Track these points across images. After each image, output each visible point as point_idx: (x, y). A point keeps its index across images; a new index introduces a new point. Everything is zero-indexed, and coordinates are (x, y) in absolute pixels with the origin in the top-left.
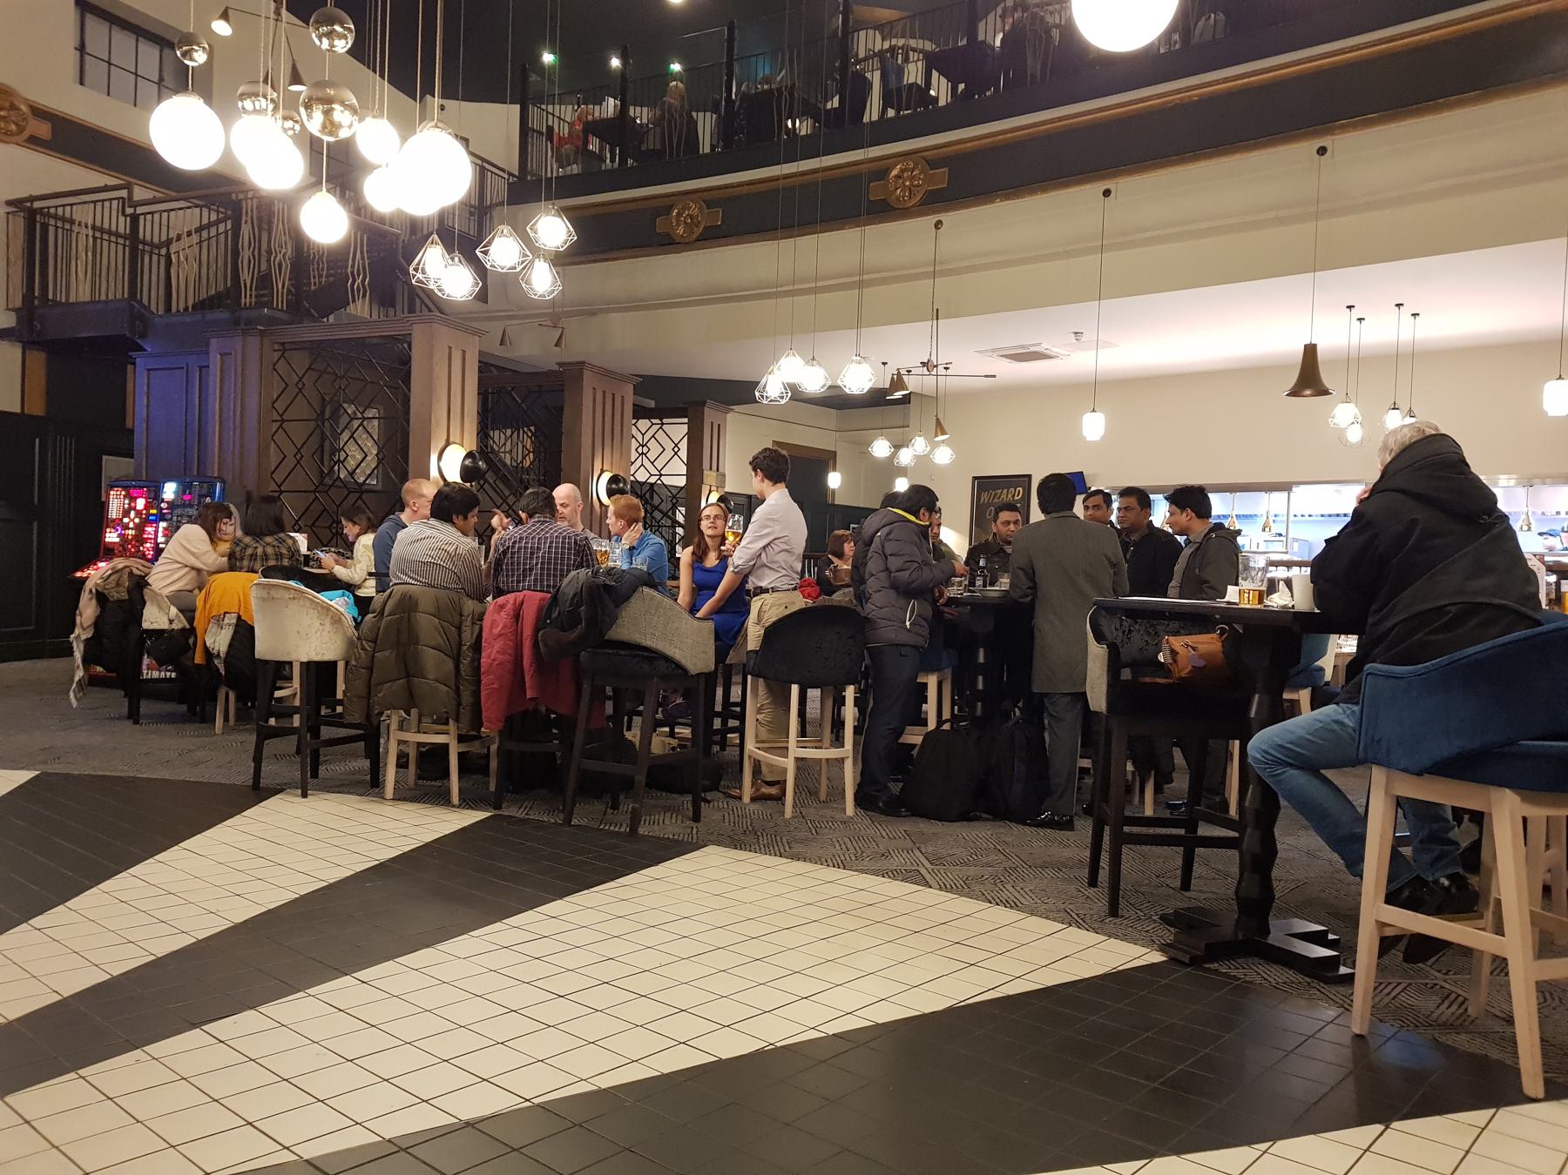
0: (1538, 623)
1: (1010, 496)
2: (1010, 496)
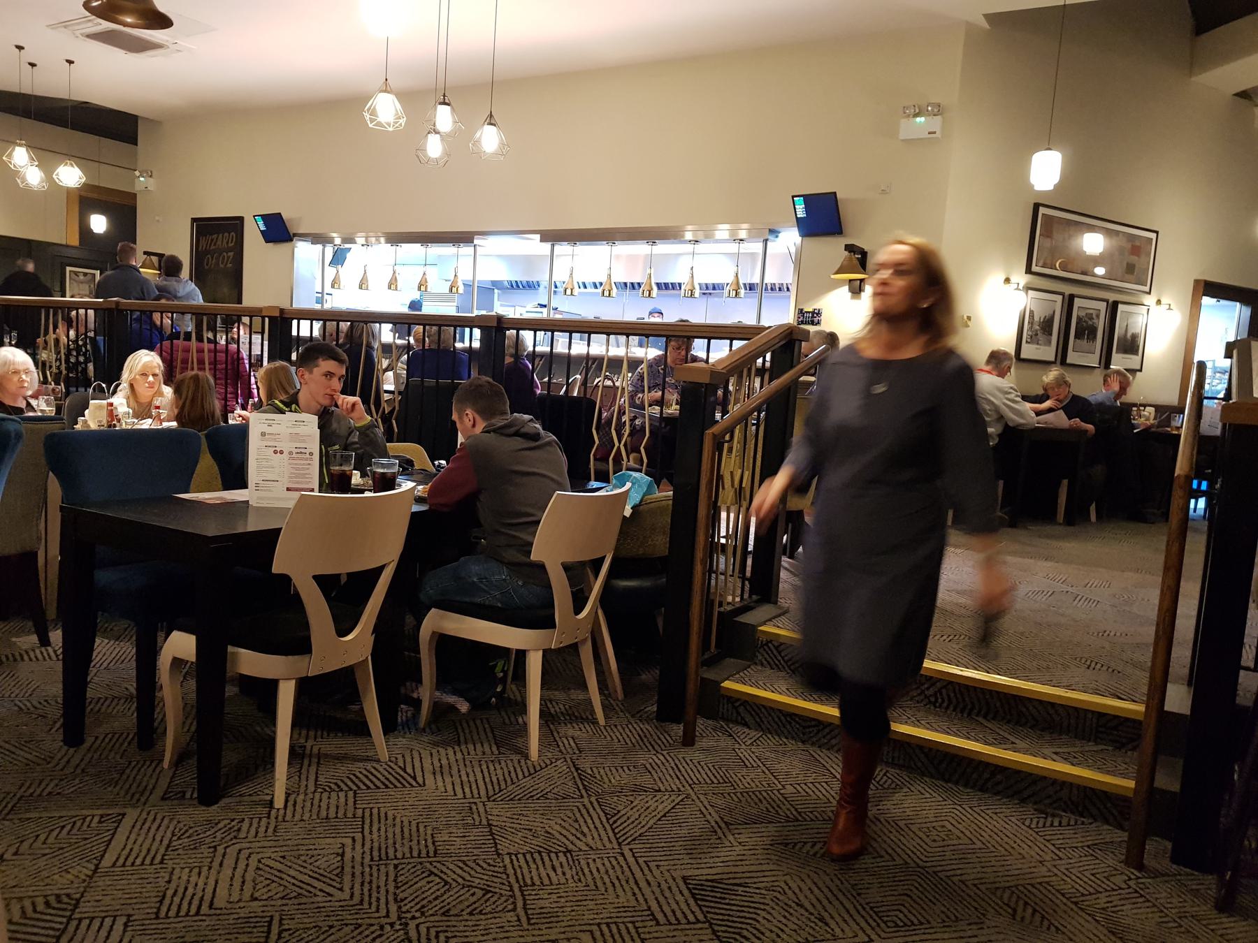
0: (176, 297)
1: (225, 241)
2: (225, 241)
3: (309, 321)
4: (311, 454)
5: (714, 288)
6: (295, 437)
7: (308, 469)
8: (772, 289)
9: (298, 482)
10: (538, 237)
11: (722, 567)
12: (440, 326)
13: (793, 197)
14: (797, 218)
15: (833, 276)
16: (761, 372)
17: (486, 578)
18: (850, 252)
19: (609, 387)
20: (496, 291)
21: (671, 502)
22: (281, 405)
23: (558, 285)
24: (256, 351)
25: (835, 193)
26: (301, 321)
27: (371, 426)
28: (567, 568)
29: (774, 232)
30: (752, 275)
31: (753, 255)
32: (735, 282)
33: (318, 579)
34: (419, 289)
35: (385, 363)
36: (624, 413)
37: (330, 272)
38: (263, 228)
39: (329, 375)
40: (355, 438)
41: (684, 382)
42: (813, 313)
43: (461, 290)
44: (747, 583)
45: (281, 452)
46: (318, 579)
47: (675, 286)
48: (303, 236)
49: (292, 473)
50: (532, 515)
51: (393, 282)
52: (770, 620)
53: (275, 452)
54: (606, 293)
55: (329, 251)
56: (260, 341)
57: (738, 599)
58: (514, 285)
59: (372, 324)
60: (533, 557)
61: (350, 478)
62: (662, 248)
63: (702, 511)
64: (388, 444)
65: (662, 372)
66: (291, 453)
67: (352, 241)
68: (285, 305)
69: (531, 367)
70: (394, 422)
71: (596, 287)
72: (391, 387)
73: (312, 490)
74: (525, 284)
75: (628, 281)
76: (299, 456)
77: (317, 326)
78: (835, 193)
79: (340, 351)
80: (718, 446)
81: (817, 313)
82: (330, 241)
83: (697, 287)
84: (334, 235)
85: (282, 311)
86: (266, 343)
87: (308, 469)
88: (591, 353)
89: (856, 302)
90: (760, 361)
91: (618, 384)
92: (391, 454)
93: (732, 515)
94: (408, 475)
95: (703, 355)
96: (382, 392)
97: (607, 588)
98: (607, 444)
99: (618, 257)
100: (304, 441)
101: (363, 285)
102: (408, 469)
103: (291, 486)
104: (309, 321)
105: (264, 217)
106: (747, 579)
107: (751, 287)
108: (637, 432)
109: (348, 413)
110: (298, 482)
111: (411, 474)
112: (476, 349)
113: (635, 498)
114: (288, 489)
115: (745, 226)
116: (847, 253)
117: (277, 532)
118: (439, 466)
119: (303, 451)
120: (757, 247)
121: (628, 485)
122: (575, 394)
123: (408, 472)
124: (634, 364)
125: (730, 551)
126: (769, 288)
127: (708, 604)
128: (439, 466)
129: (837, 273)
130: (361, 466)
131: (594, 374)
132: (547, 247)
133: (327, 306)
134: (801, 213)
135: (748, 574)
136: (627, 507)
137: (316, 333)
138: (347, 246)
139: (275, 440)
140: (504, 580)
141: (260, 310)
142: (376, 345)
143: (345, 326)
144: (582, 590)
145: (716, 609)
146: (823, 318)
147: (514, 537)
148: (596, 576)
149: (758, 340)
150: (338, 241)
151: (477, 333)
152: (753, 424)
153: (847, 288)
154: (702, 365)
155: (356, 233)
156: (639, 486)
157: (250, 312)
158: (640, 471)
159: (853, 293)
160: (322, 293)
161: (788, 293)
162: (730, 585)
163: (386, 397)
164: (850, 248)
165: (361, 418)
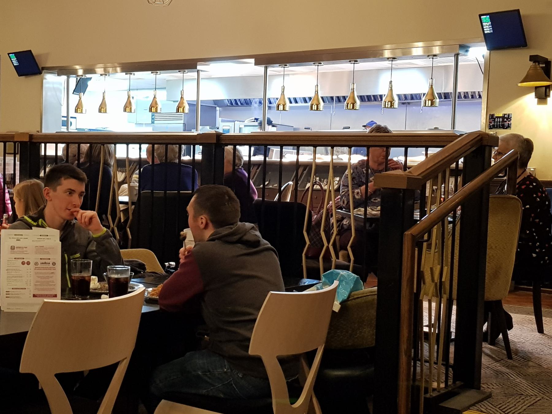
3: (54, 145)
4: (54, 264)
5: (412, 98)
6: (40, 250)
7: (51, 277)
8: (465, 97)
9: (43, 289)
10: (253, 61)
11: (426, 353)
12: (167, 144)
13: (480, 16)
14: (484, 34)
15: (520, 85)
16: (456, 173)
17: (209, 371)
18: (535, 62)
19: (317, 190)
20: (218, 108)
21: (376, 297)
22: (30, 220)
23: (272, 101)
24: (10, 171)
25: (518, 11)
26: (48, 145)
27: (106, 237)
28: (282, 361)
29: (464, 47)
30: (446, 86)
31: (446, 68)
32: (430, 92)
33: (61, 377)
34: (150, 110)
35: (120, 176)
36: (332, 215)
37: (74, 99)
38: (16, 64)
39: (71, 192)
40: (93, 247)
41: (384, 188)
42: (503, 117)
43: (186, 110)
44: (451, 369)
45: (28, 263)
46: (61, 377)
47: (377, 98)
48: (51, 70)
49: (37, 282)
50: (250, 314)
51: (128, 105)
52: (474, 405)
53: (23, 263)
54: (315, 107)
55: (73, 81)
56: (13, 162)
57: (442, 385)
58: (234, 102)
59: (109, 145)
60: (251, 352)
61: (88, 283)
62: (363, 65)
63: (405, 306)
64: (121, 250)
65: (365, 172)
66: (36, 264)
67: (92, 71)
68: (33, 130)
69: (247, 175)
70: (128, 230)
71: (305, 101)
72: (126, 199)
73: (55, 296)
74: (243, 101)
75: (335, 95)
76: (44, 266)
77: (61, 146)
78: (518, 11)
79: (79, 170)
80: (418, 243)
81: (507, 118)
82: (74, 72)
83: (396, 98)
84: (77, 67)
85: (31, 136)
86: (18, 163)
87: (51, 277)
88: (300, 160)
89: (542, 106)
90: (454, 165)
91: (326, 187)
92: (125, 259)
93: (434, 305)
94: (140, 277)
95: (402, 159)
96: (117, 203)
97: (320, 378)
98: (317, 244)
99: (324, 74)
100: (48, 253)
101: (102, 108)
102: (140, 272)
103: (36, 293)
104: (54, 145)
105: (17, 54)
106: (451, 366)
107: (446, 96)
108: (344, 231)
109: (87, 226)
110: (43, 289)
111: (142, 277)
112: (198, 160)
113: (343, 294)
114: (34, 296)
115: (439, 43)
116: (531, 63)
117: (26, 333)
118: (169, 267)
119: (47, 261)
120: (450, 61)
121: (336, 283)
122: (288, 200)
123: (140, 275)
124: (340, 169)
125: (433, 339)
126: (462, 96)
127: (414, 391)
128: (169, 267)
129: (523, 81)
130: (98, 272)
131: (306, 180)
132: (260, 69)
133: (72, 129)
134: (488, 29)
135: (451, 361)
136: (335, 302)
137: (60, 153)
138: (88, 76)
139: (23, 252)
140: (226, 372)
141: (12, 136)
142: (112, 162)
143: (85, 147)
144: (297, 381)
145: (423, 396)
146: (513, 122)
147: (235, 332)
148: (310, 365)
149: (451, 146)
150: (80, 72)
151: (199, 148)
152: (450, 222)
153: (533, 94)
154: (399, 172)
155: (95, 65)
156: (347, 283)
157: (3, 138)
158: (346, 268)
159: (539, 98)
160: (67, 117)
161: (480, 100)
162: (434, 371)
163: (122, 207)
164: (534, 59)
165: (98, 230)
